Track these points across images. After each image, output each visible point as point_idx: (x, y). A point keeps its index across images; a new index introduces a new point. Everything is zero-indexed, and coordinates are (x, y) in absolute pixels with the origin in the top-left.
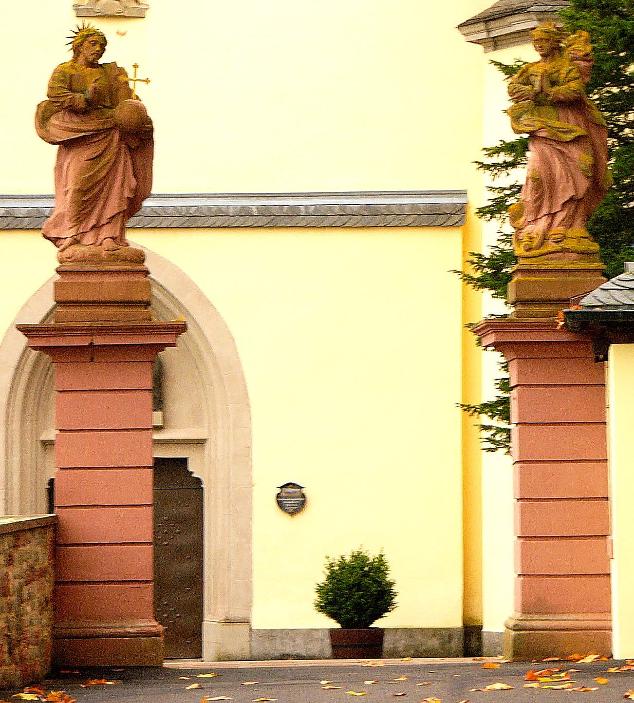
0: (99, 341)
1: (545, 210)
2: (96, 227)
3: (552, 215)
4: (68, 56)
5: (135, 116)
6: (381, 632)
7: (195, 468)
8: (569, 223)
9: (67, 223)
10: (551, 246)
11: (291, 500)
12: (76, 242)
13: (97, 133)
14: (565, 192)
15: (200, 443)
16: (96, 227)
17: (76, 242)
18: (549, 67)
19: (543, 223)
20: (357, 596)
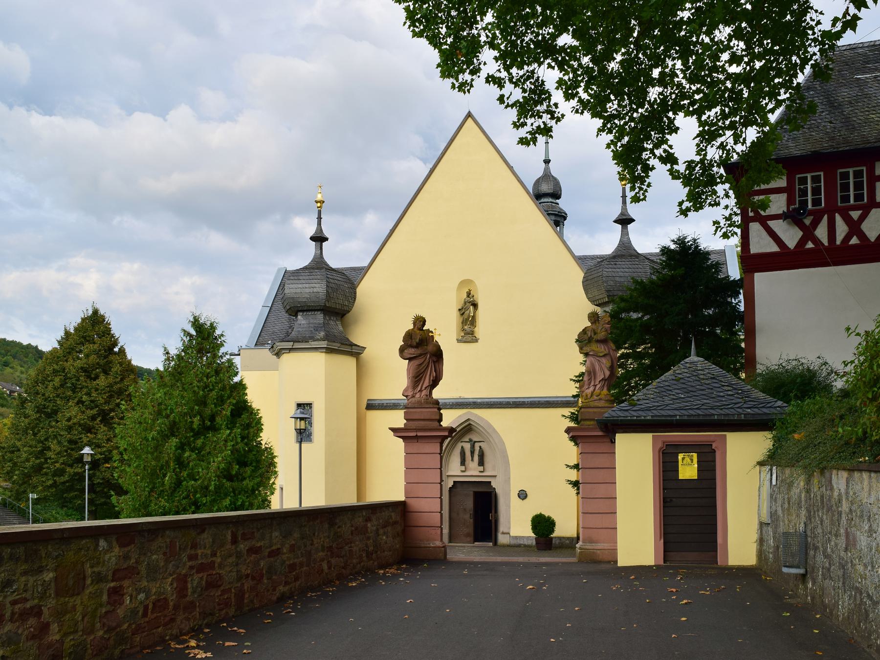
0: (419, 434)
1: (592, 383)
2: (421, 391)
3: (595, 386)
4: (411, 327)
5: (435, 349)
6: (552, 538)
7: (493, 484)
8: (602, 388)
9: (410, 390)
10: (595, 397)
11: (523, 495)
12: (413, 397)
13: (420, 355)
14: (600, 376)
15: (495, 476)
16: (421, 391)
17: (413, 397)
18: (594, 327)
19: (592, 389)
20: (543, 525)
